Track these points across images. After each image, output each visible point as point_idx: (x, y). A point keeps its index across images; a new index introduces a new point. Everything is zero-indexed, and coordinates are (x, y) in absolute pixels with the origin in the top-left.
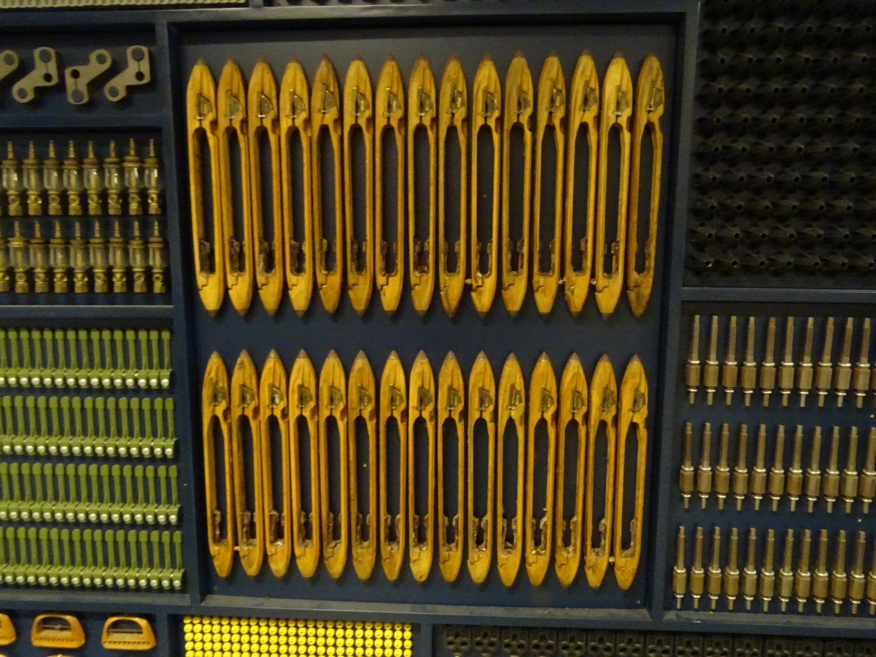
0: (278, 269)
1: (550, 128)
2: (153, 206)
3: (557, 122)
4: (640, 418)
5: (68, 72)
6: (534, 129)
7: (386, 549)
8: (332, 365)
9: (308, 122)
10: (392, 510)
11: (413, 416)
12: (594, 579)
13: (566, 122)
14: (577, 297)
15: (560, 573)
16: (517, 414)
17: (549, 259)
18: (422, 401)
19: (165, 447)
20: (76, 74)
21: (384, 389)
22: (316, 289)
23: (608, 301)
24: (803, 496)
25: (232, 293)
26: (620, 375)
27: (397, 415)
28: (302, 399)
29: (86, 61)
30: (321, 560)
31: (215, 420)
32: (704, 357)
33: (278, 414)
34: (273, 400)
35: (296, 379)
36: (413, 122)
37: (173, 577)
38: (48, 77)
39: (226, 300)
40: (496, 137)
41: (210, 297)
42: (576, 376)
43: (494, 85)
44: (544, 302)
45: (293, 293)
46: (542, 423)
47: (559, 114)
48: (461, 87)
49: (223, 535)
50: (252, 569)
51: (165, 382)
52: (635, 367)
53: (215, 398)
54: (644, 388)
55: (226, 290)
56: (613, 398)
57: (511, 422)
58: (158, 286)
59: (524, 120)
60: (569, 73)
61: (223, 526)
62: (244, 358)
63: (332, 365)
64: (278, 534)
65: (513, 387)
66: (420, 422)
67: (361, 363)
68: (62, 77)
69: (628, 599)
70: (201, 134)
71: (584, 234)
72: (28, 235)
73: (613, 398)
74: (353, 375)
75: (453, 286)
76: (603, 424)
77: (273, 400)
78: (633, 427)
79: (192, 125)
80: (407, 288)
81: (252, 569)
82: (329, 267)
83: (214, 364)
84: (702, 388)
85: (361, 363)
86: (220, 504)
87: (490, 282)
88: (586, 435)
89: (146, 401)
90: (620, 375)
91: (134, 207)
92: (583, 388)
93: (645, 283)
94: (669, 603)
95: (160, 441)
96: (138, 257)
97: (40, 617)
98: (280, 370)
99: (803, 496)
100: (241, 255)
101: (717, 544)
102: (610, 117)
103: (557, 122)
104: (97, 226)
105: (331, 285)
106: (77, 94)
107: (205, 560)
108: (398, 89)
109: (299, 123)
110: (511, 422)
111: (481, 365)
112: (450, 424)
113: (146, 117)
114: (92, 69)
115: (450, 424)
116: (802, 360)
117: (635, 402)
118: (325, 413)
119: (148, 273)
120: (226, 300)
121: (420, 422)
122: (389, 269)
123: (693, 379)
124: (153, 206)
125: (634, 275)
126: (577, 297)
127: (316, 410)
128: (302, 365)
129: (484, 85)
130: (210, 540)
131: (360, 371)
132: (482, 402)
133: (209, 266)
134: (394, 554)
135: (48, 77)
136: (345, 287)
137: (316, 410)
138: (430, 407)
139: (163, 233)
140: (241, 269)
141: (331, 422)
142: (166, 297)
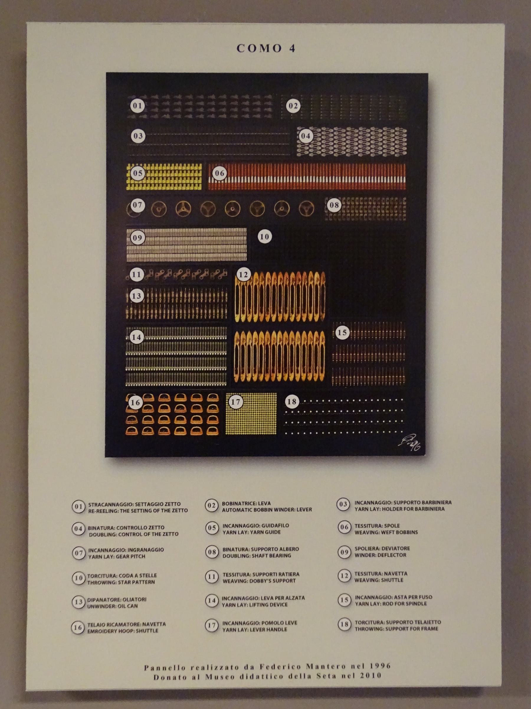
1: (304, 285)
3: (306, 284)
4: (324, 343)
6: (240, 286)
8: (261, 333)
9: (259, 284)
11: (253, 344)
13: (307, 284)
14: (310, 319)
15: (308, 378)
16: (299, 343)
17: (305, 311)
22: (259, 317)
23: (316, 319)
25: (242, 318)
26: (319, 334)
29: (196, 272)
30: (258, 377)
31: (237, 346)
36: (279, 284)
39: (240, 320)
40: (294, 287)
41: (237, 320)
43: (294, 277)
44: (304, 320)
46: (304, 345)
47: (306, 282)
48: (288, 277)
51: (226, 338)
54: (324, 337)
56: (318, 339)
57: (298, 345)
60: (308, 275)
63: (261, 333)
64: (249, 372)
66: (255, 346)
67: (267, 333)
70: (237, 286)
71: (311, 306)
73: (318, 339)
74: (266, 336)
76: (316, 345)
78: (322, 345)
79: (236, 285)
80: (277, 317)
82: (262, 313)
83: (237, 334)
85: (267, 333)
87: (294, 315)
88: (313, 348)
89: (157, 343)
90: (319, 334)
92: (312, 337)
102: (315, 283)
103: (306, 284)
105: (262, 316)
108: (276, 277)
109: (257, 284)
110: (298, 345)
111: (292, 333)
112: (285, 345)
114: (197, 273)
115: (285, 345)
120: (240, 320)
121: (255, 346)
122: (274, 313)
126: (310, 319)
128: (255, 333)
130: (234, 373)
133: (237, 313)
135: (175, 274)
136: (265, 317)
138: (281, 342)
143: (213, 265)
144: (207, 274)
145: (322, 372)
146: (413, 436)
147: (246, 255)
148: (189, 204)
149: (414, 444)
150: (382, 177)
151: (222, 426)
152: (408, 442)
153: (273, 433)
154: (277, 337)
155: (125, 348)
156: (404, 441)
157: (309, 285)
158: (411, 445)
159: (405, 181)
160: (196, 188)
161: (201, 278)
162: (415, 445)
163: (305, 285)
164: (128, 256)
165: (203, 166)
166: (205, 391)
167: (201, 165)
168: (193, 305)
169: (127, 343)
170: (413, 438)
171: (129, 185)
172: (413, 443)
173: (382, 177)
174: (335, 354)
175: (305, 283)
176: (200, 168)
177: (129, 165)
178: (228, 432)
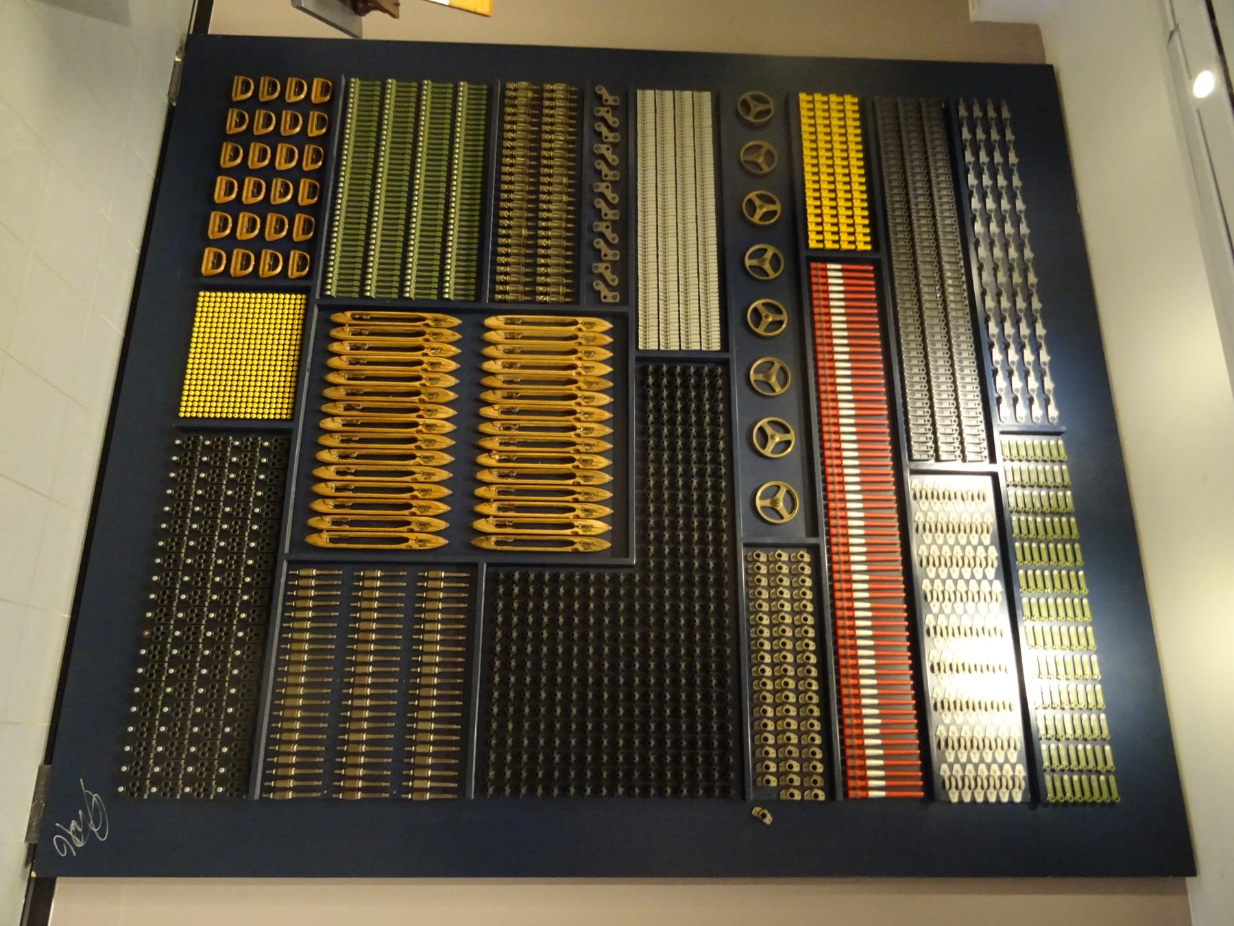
0: (505, 356)
2: (541, 298)
3: (576, 496)
5: (608, 265)
7: (331, 503)
8: (453, 381)
10: (356, 490)
12: (313, 522)
13: (576, 501)
18: (422, 524)
19: (410, 292)
20: (607, 268)
21: (436, 407)
23: (480, 525)
24: (358, 641)
26: (438, 533)
27: (413, 510)
28: (432, 364)
31: (423, 319)
32: (445, 579)
33: (425, 351)
34: (433, 349)
35: (444, 361)
37: (332, 291)
38: (606, 176)
39: (490, 329)
41: (491, 321)
42: (438, 508)
45: (491, 362)
49: (354, 319)
50: (334, 333)
52: (442, 541)
53: (436, 320)
54: (429, 546)
55: (495, 330)
58: (499, 297)
59: (578, 479)
61: (361, 319)
62: (458, 336)
63: (453, 381)
65: (434, 474)
68: (607, 181)
69: (299, 543)
70: (575, 323)
71: (517, 511)
72: (529, 237)
75: (491, 509)
77: (433, 349)
78: (406, 540)
79: (580, 319)
81: (334, 333)
83: (456, 321)
84: (427, 579)
86: (373, 319)
90: (438, 533)
91: (541, 289)
93: (491, 544)
94: (293, 564)
95: (413, 291)
96: (516, 251)
97: (308, 257)
98: (444, 446)
99: (358, 641)
100: (513, 338)
101: (314, 737)
104: (531, 242)
106: (597, 268)
107: (343, 309)
109: (579, 370)
113: (585, 297)
116: (436, 712)
117: (421, 541)
118: (424, 375)
119: (506, 292)
123: (432, 574)
124: (541, 298)
125: (493, 539)
127: (425, 370)
128: (453, 365)
129: (595, 459)
131: (448, 395)
132: (426, 457)
134: (339, 409)
135: (607, 187)
137: (425, 370)
139: (526, 302)
140: (503, 413)
141: (419, 378)
142: (492, 300)
143: (627, 270)
144: (607, 101)
145: (332, 540)
146: (102, 833)
147: (653, 346)
148: (773, 221)
149: (76, 832)
150: (879, 721)
151: (225, 283)
152: (85, 813)
153: (183, 409)
154: (442, 418)
155: (477, 83)
156: (90, 798)
157: (574, 505)
158: (73, 824)
159: (872, 794)
160: (813, 237)
161: (598, 243)
162: (73, 837)
163: (573, 493)
164: (650, 94)
165: (865, 251)
166: (314, 248)
167: (869, 247)
168: (533, 220)
169: (451, 85)
170: (95, 830)
171: (840, 99)
172: (80, 830)
173: (879, 721)
174: (381, 579)
175: (580, 493)
176: (861, 247)
177: (856, 100)
178: (206, 300)
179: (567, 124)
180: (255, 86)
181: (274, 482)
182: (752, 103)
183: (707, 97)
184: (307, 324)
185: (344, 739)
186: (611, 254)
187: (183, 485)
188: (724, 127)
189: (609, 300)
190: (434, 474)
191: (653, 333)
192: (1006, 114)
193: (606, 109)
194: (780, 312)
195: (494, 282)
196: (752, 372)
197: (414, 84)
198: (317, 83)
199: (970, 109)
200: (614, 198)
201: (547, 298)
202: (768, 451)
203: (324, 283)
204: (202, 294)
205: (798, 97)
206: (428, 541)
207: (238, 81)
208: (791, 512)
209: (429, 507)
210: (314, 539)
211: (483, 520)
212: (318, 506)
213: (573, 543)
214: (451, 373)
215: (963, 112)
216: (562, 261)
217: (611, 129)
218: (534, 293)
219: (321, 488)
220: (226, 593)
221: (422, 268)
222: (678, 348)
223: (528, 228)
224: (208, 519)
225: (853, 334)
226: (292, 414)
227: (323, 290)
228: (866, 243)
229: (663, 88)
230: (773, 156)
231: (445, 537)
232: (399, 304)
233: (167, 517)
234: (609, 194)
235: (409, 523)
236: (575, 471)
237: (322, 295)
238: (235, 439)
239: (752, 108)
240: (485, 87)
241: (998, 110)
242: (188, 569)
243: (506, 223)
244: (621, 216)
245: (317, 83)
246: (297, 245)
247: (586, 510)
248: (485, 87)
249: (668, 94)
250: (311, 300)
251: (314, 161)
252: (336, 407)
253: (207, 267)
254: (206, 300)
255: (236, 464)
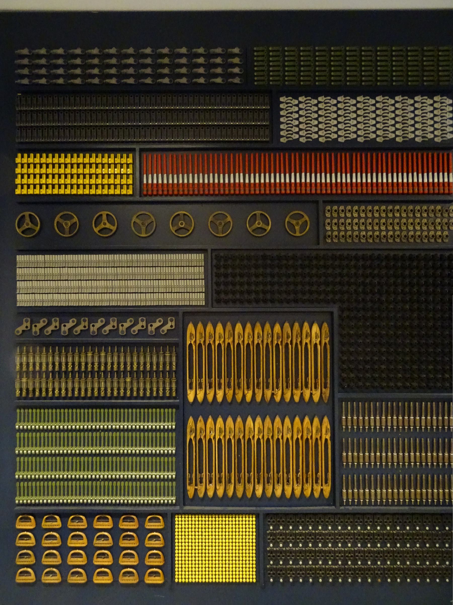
3: (298, 343)
8: (230, 420)
10: (249, 472)
13: (301, 342)
23: (316, 398)
31: (191, 440)
37: (173, 499)
41: (191, 397)
42: (308, 422)
52: (326, 420)
54: (329, 427)
58: (174, 394)
63: (230, 420)
70: (191, 345)
72: (28, 377)
78: (326, 440)
79: (188, 343)
81: (201, 495)
83: (191, 421)
93: (327, 392)
104: (135, 375)
107: (185, 491)
125: (324, 390)
131: (239, 422)
147: (203, 296)
176: (130, 161)
177: (19, 155)
178: (180, 577)
179: (47, 354)
180: (74, 568)
181: (313, 520)
182: (25, 227)
183: (20, 258)
184: (199, 512)
185: (352, 465)
186: (113, 323)
187: (296, 572)
188: (117, 246)
189: (173, 324)
190: (288, 427)
191: (194, 296)
192: (25, 51)
193: (33, 327)
194: (23, 217)
195: (131, 398)
196: (64, 236)
197: (18, 459)
198: (20, 525)
199: (23, 77)
200: (44, 322)
201: (174, 363)
202: (114, 228)
203: (168, 505)
204: (176, 580)
205: (18, 195)
206: (327, 427)
207: (20, 579)
208: (101, 215)
209: (278, 428)
210: (327, 494)
211: (314, 396)
212: (308, 493)
213: (325, 344)
214: (225, 421)
215: (25, 81)
216: (116, 354)
217: (49, 324)
218: (170, 372)
219: (298, 492)
220: (357, 539)
221: (166, 444)
222: (203, 281)
223: (125, 377)
224: (315, 555)
225: (359, 170)
226: (252, 514)
227: (172, 505)
228: (128, 157)
229: (15, 288)
230: (64, 215)
231: (275, 418)
232: (181, 457)
233: (316, 579)
234: (41, 325)
235: (317, 439)
236: (284, 344)
237: (175, 505)
238: (269, 546)
239: (29, 227)
240: (18, 411)
241: (22, 57)
242: (345, 562)
243: (122, 391)
244: (85, 316)
245: (20, 525)
246: (142, 525)
247: (307, 336)
248: (18, 411)
249: (19, 284)
250: (181, 512)
251: (56, 520)
252: (316, 490)
253: (159, 580)
254: (180, 577)
255: (284, 544)
